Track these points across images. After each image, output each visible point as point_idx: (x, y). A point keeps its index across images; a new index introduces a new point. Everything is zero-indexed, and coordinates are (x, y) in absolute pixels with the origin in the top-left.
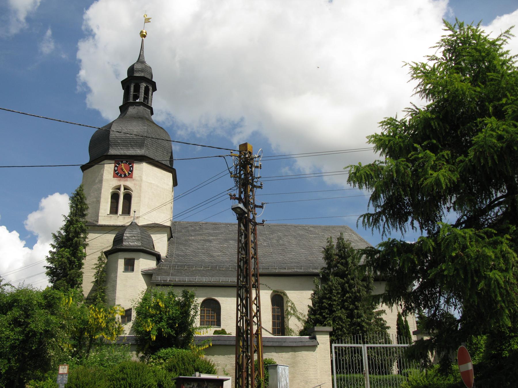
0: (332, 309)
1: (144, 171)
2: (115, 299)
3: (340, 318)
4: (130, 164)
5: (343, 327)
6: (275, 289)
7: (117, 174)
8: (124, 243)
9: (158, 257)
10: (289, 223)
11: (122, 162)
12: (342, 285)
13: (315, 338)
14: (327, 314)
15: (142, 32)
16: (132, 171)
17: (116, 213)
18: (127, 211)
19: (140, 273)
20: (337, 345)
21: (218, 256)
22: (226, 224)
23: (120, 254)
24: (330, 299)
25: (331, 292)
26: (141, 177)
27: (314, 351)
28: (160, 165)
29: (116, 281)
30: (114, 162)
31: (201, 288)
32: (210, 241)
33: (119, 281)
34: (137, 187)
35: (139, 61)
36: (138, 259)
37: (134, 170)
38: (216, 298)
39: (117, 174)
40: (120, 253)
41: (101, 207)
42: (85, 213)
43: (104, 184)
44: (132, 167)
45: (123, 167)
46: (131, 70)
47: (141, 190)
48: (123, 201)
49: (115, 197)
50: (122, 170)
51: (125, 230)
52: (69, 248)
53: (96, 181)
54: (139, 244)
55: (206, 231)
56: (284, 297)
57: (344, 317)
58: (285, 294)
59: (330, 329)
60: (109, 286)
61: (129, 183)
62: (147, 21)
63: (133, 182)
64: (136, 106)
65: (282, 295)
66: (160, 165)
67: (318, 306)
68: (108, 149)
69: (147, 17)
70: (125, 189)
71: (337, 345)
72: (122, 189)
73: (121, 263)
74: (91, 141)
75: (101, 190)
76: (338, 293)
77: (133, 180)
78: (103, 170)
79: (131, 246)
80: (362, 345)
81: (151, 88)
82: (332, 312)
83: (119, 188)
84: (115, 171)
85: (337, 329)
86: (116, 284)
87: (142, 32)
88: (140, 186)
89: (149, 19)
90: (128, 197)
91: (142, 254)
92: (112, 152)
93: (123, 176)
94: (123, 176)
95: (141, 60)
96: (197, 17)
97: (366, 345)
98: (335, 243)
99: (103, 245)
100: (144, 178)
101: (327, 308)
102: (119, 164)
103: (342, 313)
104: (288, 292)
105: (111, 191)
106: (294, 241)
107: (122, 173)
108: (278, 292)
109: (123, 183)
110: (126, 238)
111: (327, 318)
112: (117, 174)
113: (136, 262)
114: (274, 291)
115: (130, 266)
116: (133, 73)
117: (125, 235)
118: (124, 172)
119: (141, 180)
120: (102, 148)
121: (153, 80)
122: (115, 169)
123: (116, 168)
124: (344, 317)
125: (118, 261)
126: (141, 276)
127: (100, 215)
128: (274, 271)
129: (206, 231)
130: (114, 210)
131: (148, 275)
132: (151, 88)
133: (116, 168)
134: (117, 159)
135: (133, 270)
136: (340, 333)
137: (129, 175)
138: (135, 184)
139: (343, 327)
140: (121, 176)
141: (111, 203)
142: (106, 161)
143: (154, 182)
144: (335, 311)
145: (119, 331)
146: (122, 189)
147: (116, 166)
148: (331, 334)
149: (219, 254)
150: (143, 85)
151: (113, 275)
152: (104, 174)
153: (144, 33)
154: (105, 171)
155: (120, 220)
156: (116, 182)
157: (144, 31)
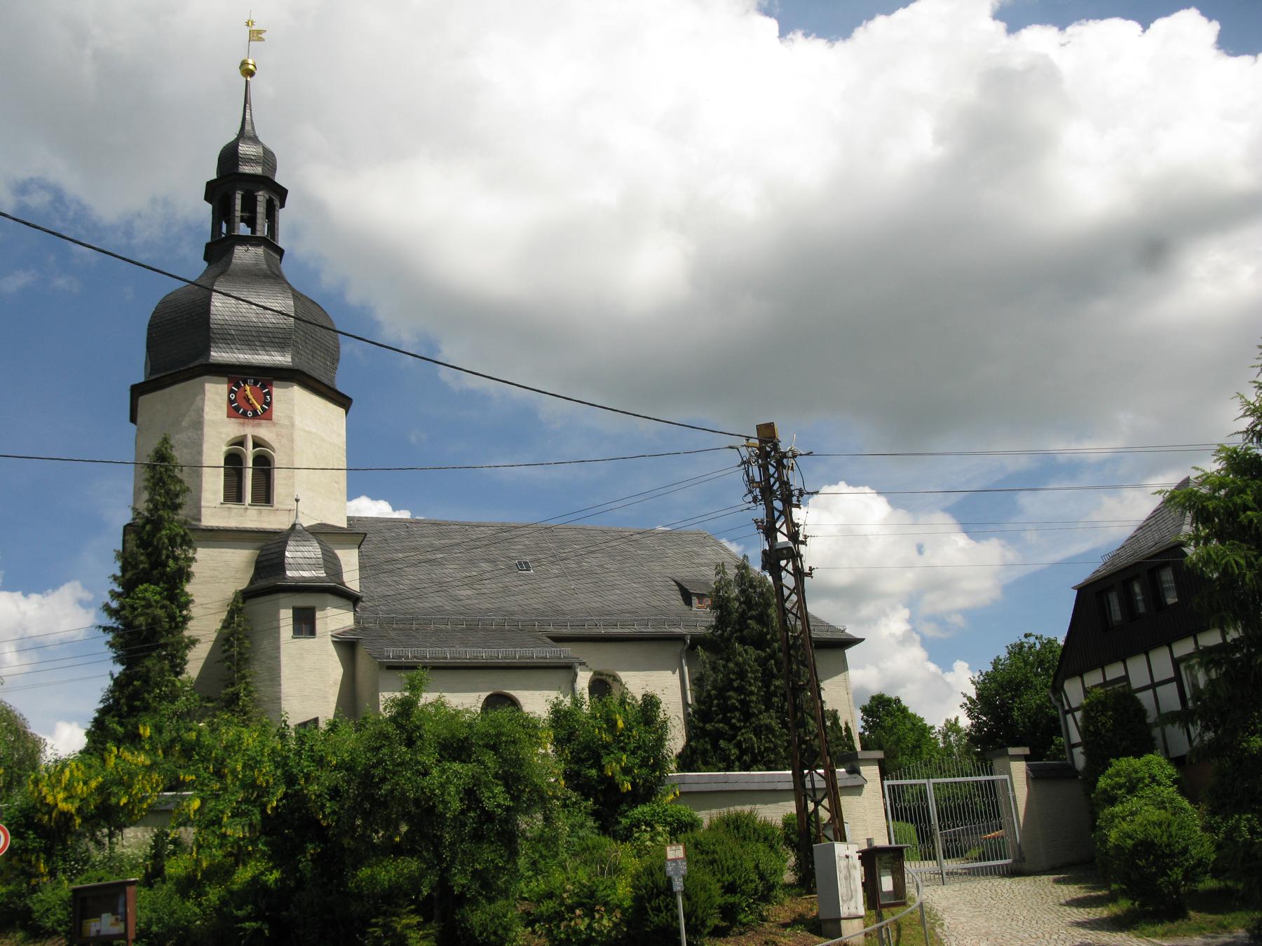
0: (748, 712)
1: (293, 401)
3: (769, 729)
4: (263, 387)
5: (776, 747)
6: (598, 669)
7: (237, 409)
8: (289, 573)
9: (352, 599)
10: (552, 523)
11: (245, 382)
12: (762, 662)
14: (739, 720)
15: (244, 63)
16: (269, 404)
18: (264, 495)
19: (330, 639)
20: (891, 782)
22: (463, 525)
23: (284, 598)
24: (740, 690)
25: (742, 675)
26: (291, 418)
28: (323, 389)
29: (278, 658)
32: (440, 563)
34: (284, 441)
35: (242, 135)
38: (513, 693)
39: (237, 410)
40: (281, 595)
41: (205, 485)
42: (178, 501)
43: (208, 431)
44: (269, 393)
45: (248, 392)
46: (229, 157)
47: (292, 449)
48: (253, 473)
49: (233, 461)
50: (248, 400)
51: (285, 543)
52: (157, 584)
54: (322, 574)
55: (424, 541)
56: (615, 686)
57: (775, 724)
58: (616, 679)
60: (256, 668)
61: (264, 431)
63: (274, 429)
64: (252, 245)
65: (610, 680)
66: (323, 389)
67: (718, 705)
69: (254, 28)
70: (256, 445)
71: (891, 782)
74: (152, 327)
75: (201, 445)
76: (756, 679)
78: (203, 400)
80: (925, 781)
81: (277, 203)
82: (747, 716)
84: (231, 402)
85: (767, 749)
87: (244, 63)
88: (291, 440)
89: (259, 32)
90: (264, 464)
91: (330, 598)
92: (219, 355)
93: (250, 414)
94: (250, 414)
95: (245, 134)
97: (932, 781)
98: (732, 573)
99: (216, 573)
100: (298, 420)
101: (736, 709)
102: (238, 386)
105: (225, 448)
108: (601, 674)
109: (251, 430)
110: (291, 561)
111: (740, 729)
112: (237, 409)
113: (318, 614)
114: (595, 673)
115: (305, 624)
116: (237, 165)
117: (287, 554)
118: (252, 405)
119: (293, 425)
121: (277, 180)
122: (229, 398)
123: (233, 397)
124: (775, 724)
125: (278, 613)
126: (331, 647)
127: (203, 504)
128: (595, 631)
129: (424, 541)
130: (233, 493)
132: (277, 203)
133: (233, 397)
134: (234, 374)
135: (312, 632)
136: (772, 757)
139: (776, 747)
140: (244, 415)
142: (206, 377)
143: (314, 430)
144: (753, 715)
146: (250, 444)
147: (231, 391)
149: (469, 592)
150: (262, 197)
152: (206, 409)
153: (251, 67)
154: (206, 403)
155: (250, 517)
156: (233, 429)
157: (250, 61)
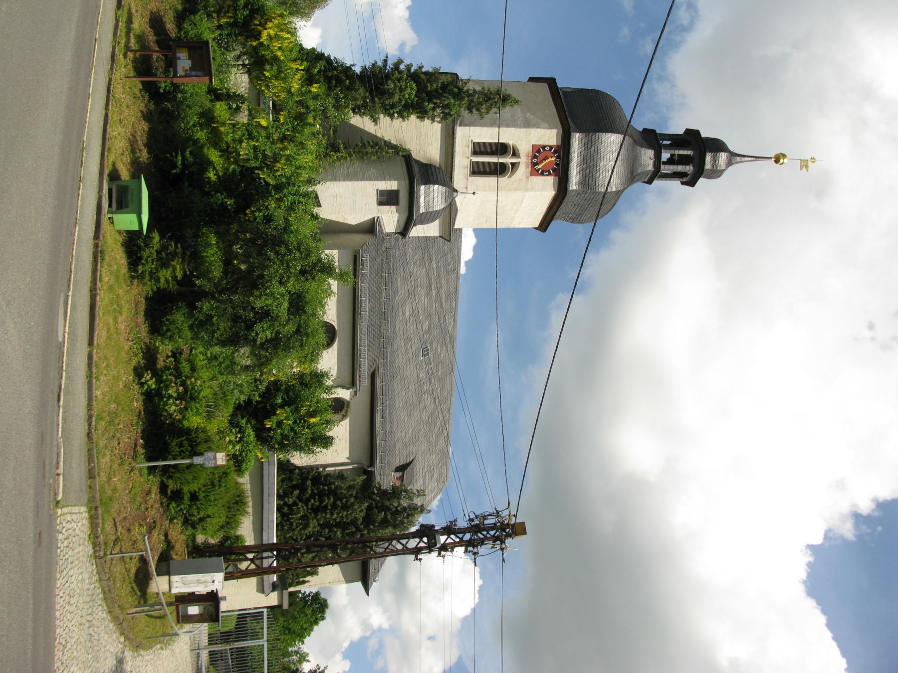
1: (543, 191)
2: (335, 180)
3: (306, 526)
4: (554, 170)
5: (293, 530)
7: (539, 151)
8: (423, 187)
9: (404, 231)
11: (557, 157)
12: (354, 522)
13: (273, 590)
14: (313, 505)
15: (784, 156)
16: (542, 174)
17: (475, 153)
18: (478, 170)
19: (376, 216)
21: (404, 313)
23: (405, 184)
24: (334, 506)
26: (532, 189)
27: (258, 591)
30: (560, 144)
31: (350, 353)
32: (428, 294)
38: (336, 344)
39: (538, 152)
40: (407, 182)
41: (485, 128)
43: (523, 131)
44: (550, 174)
45: (550, 159)
46: (717, 146)
48: (493, 162)
49: (501, 149)
51: (444, 185)
52: (416, 96)
53: (528, 115)
54: (422, 210)
55: (444, 282)
58: (344, 417)
59: (286, 606)
61: (523, 170)
62: (804, 164)
64: (654, 162)
65: (343, 412)
68: (580, 131)
69: (810, 163)
70: (513, 164)
73: (393, 185)
74: (597, 92)
75: (513, 126)
76: (342, 517)
77: (528, 178)
79: (418, 198)
81: (685, 180)
82: (316, 511)
84: (544, 147)
85: (291, 524)
86: (358, 180)
87: (784, 156)
88: (516, 190)
89: (807, 167)
90: (499, 170)
91: (405, 215)
92: (577, 139)
93: (535, 160)
94: (535, 160)
96: (867, 93)
97: (266, 644)
98: (418, 501)
102: (555, 152)
103: (314, 527)
104: (346, 423)
105: (511, 143)
106: (425, 416)
107: (541, 157)
109: (523, 161)
110: (431, 189)
112: (539, 151)
113: (393, 208)
114: (348, 402)
115: (387, 198)
116: (711, 151)
117: (436, 186)
119: (527, 190)
120: (582, 111)
123: (547, 149)
125: (395, 180)
126: (371, 217)
127: (472, 128)
129: (444, 282)
130: (479, 149)
131: (371, 228)
133: (547, 149)
134: (563, 150)
135: (381, 203)
136: (286, 528)
137: (535, 171)
139: (293, 530)
140: (535, 157)
141: (491, 143)
144: (316, 515)
146: (514, 160)
147: (551, 147)
148: (280, 606)
150: (689, 169)
151: (373, 171)
152: (538, 130)
153: (781, 161)
154: (543, 130)
155: (463, 160)
156: (525, 149)
157: (786, 160)
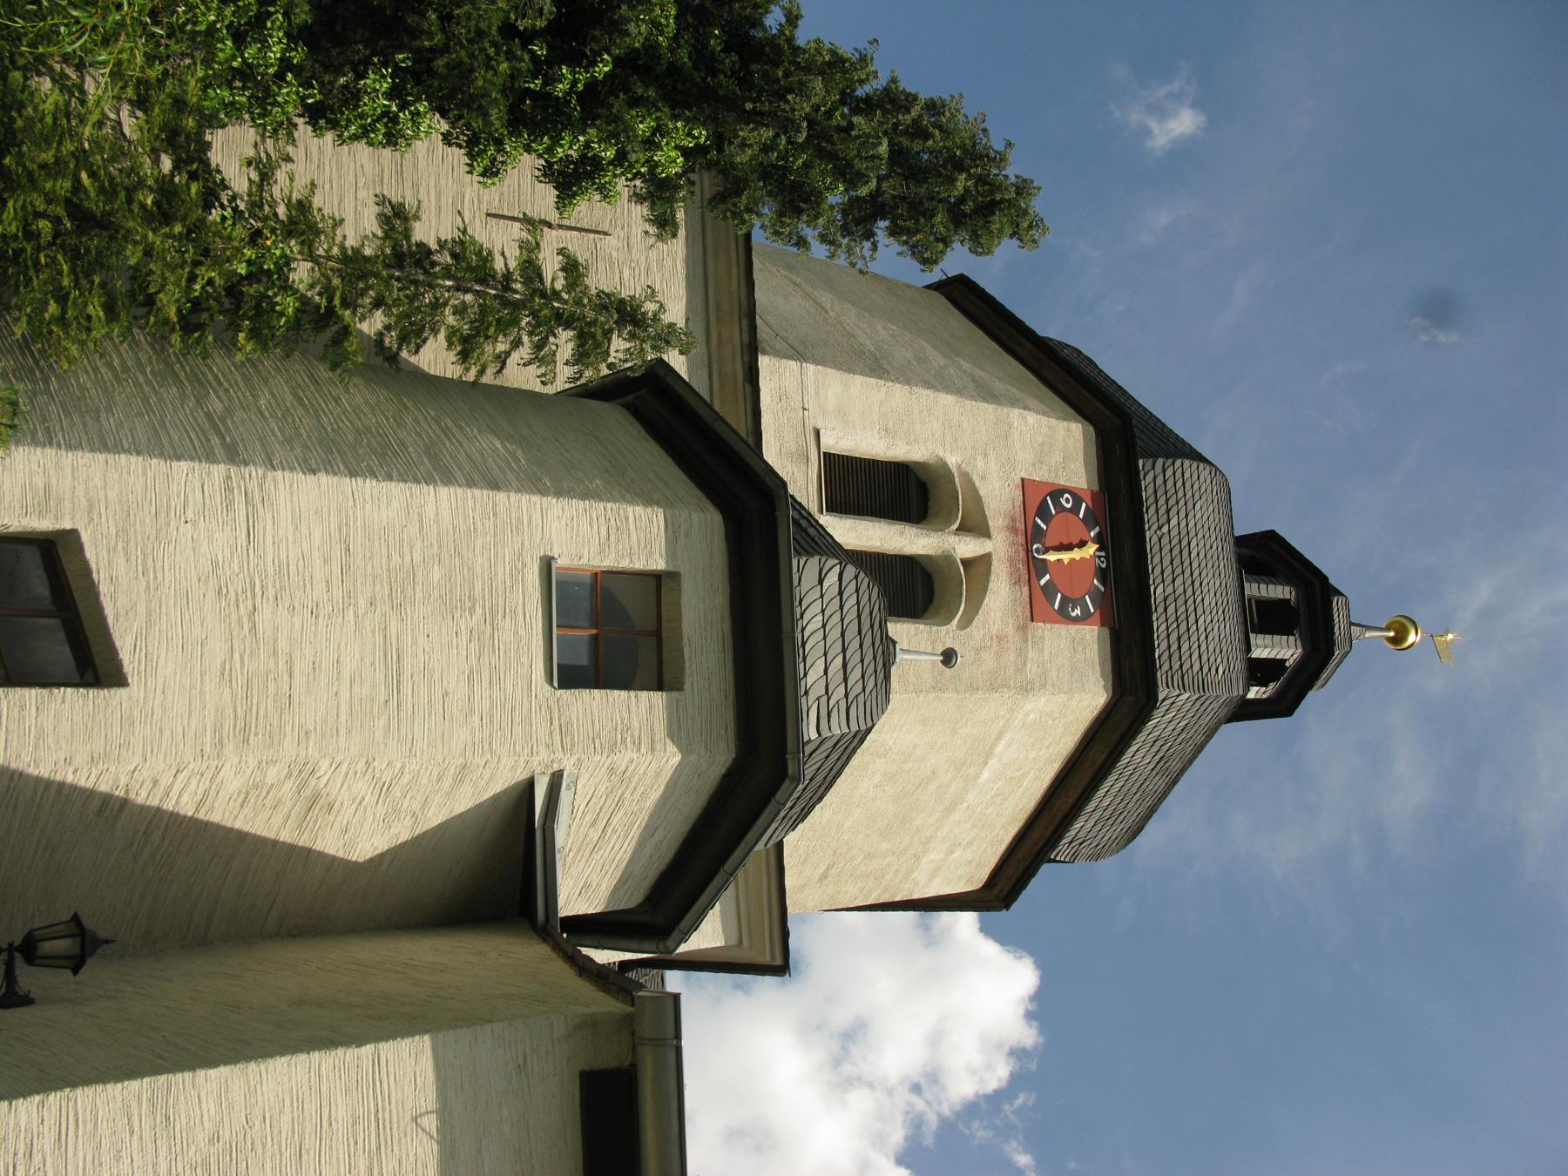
2: (234, 456)
7: (1043, 511)
30: (1096, 488)
33: (443, 503)
36: (677, 731)
37: (1073, 628)
61: (1002, 595)
63: (1010, 630)
72: (966, 547)
83: (976, 526)
84: (1057, 493)
105: (952, 461)
112: (1043, 511)
115: (607, 635)
119: (1026, 689)
126: (501, 779)
127: (811, 368)
135: (569, 677)
138: (1000, 638)
143: (985, 775)
145: (127, 258)
146: (966, 547)
156: (999, 498)
